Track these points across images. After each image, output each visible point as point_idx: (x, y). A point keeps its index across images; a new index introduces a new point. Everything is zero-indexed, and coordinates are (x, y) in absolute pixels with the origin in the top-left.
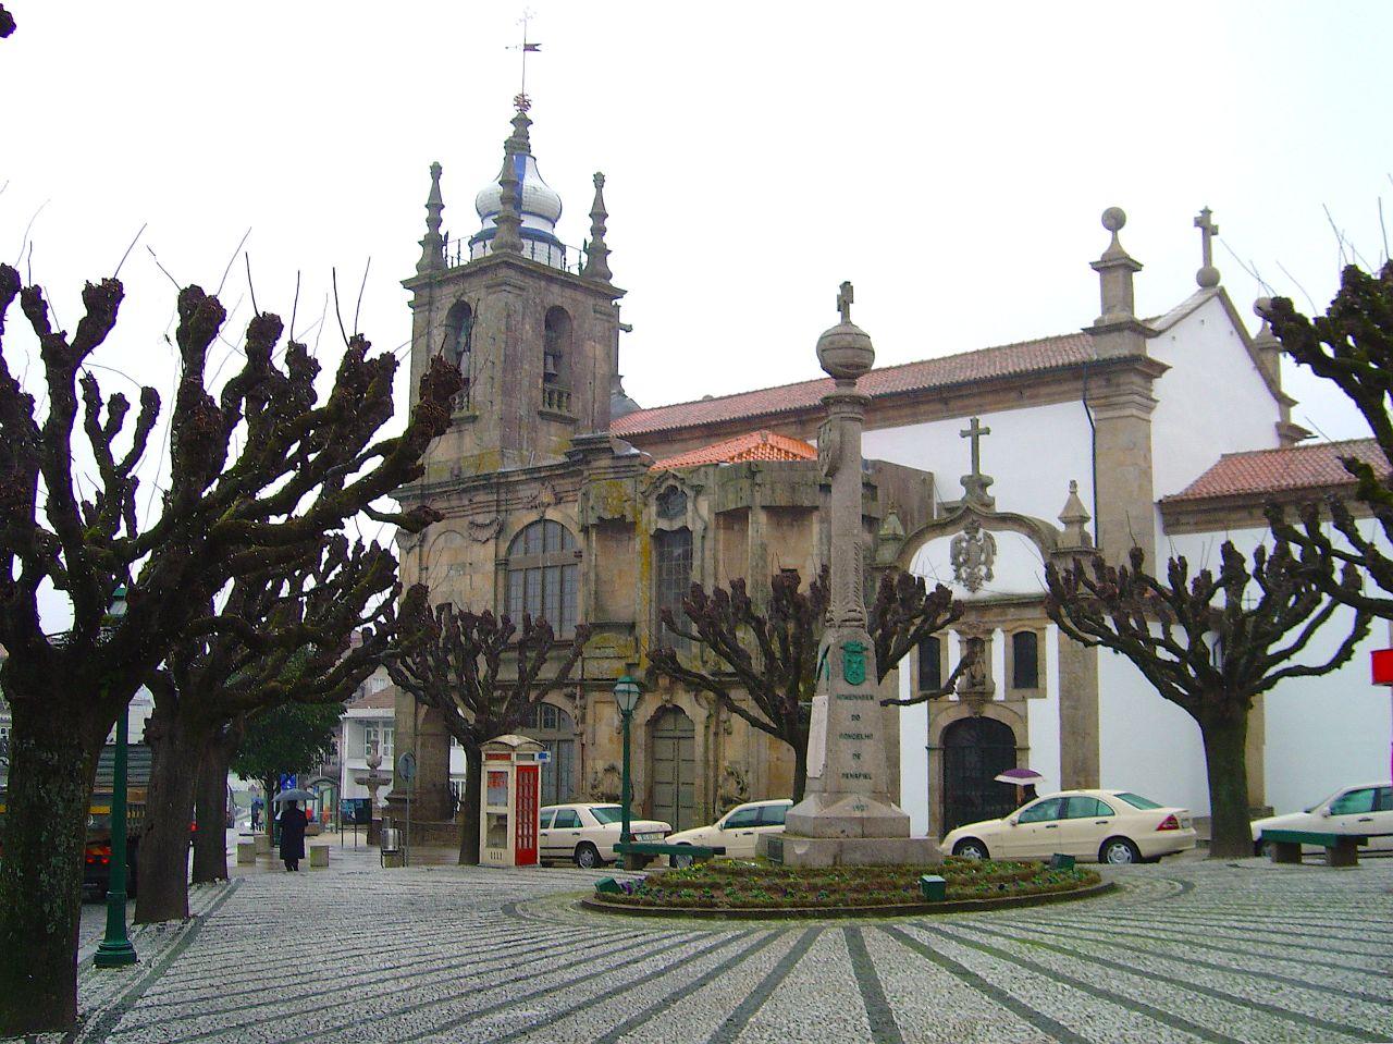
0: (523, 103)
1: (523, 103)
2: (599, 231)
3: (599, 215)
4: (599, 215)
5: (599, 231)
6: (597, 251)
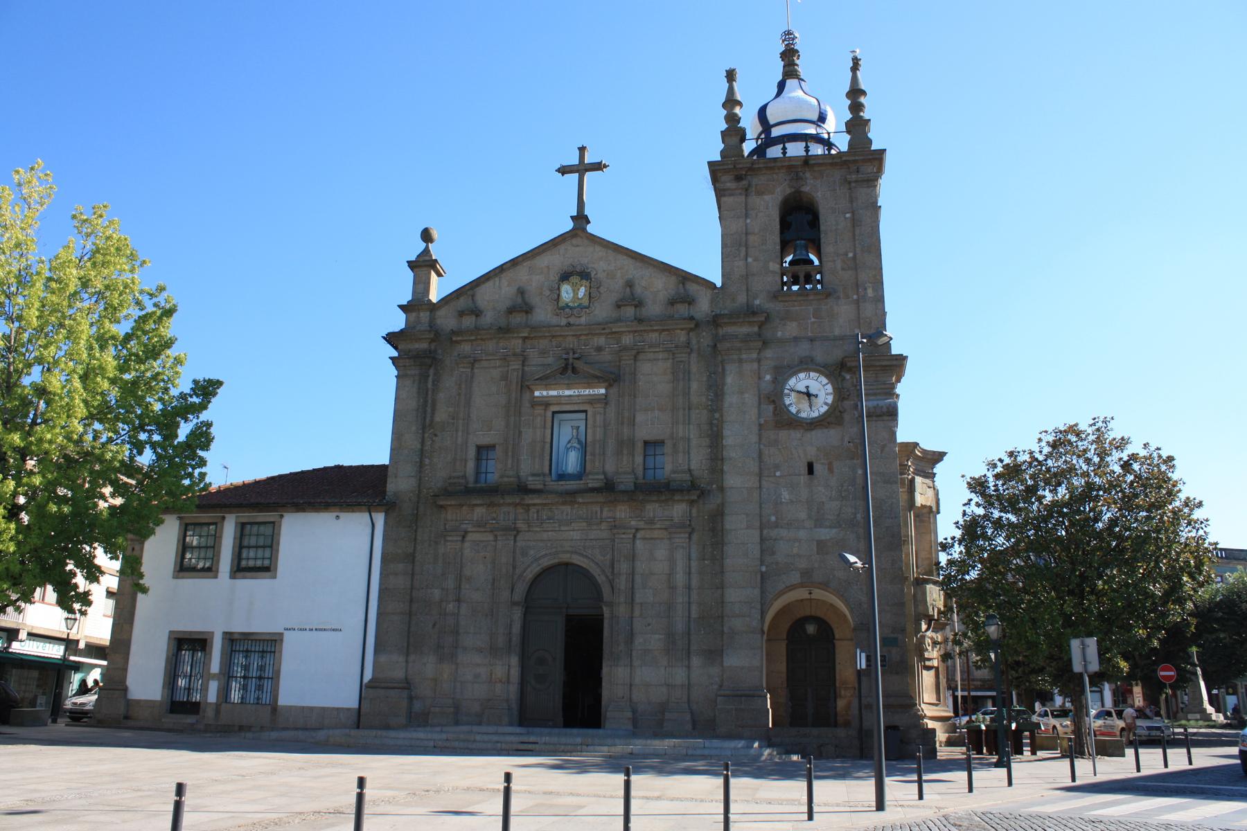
0: (788, 36)
1: (788, 36)
2: (856, 107)
3: (855, 93)
4: (855, 93)
5: (856, 107)
6: (857, 126)
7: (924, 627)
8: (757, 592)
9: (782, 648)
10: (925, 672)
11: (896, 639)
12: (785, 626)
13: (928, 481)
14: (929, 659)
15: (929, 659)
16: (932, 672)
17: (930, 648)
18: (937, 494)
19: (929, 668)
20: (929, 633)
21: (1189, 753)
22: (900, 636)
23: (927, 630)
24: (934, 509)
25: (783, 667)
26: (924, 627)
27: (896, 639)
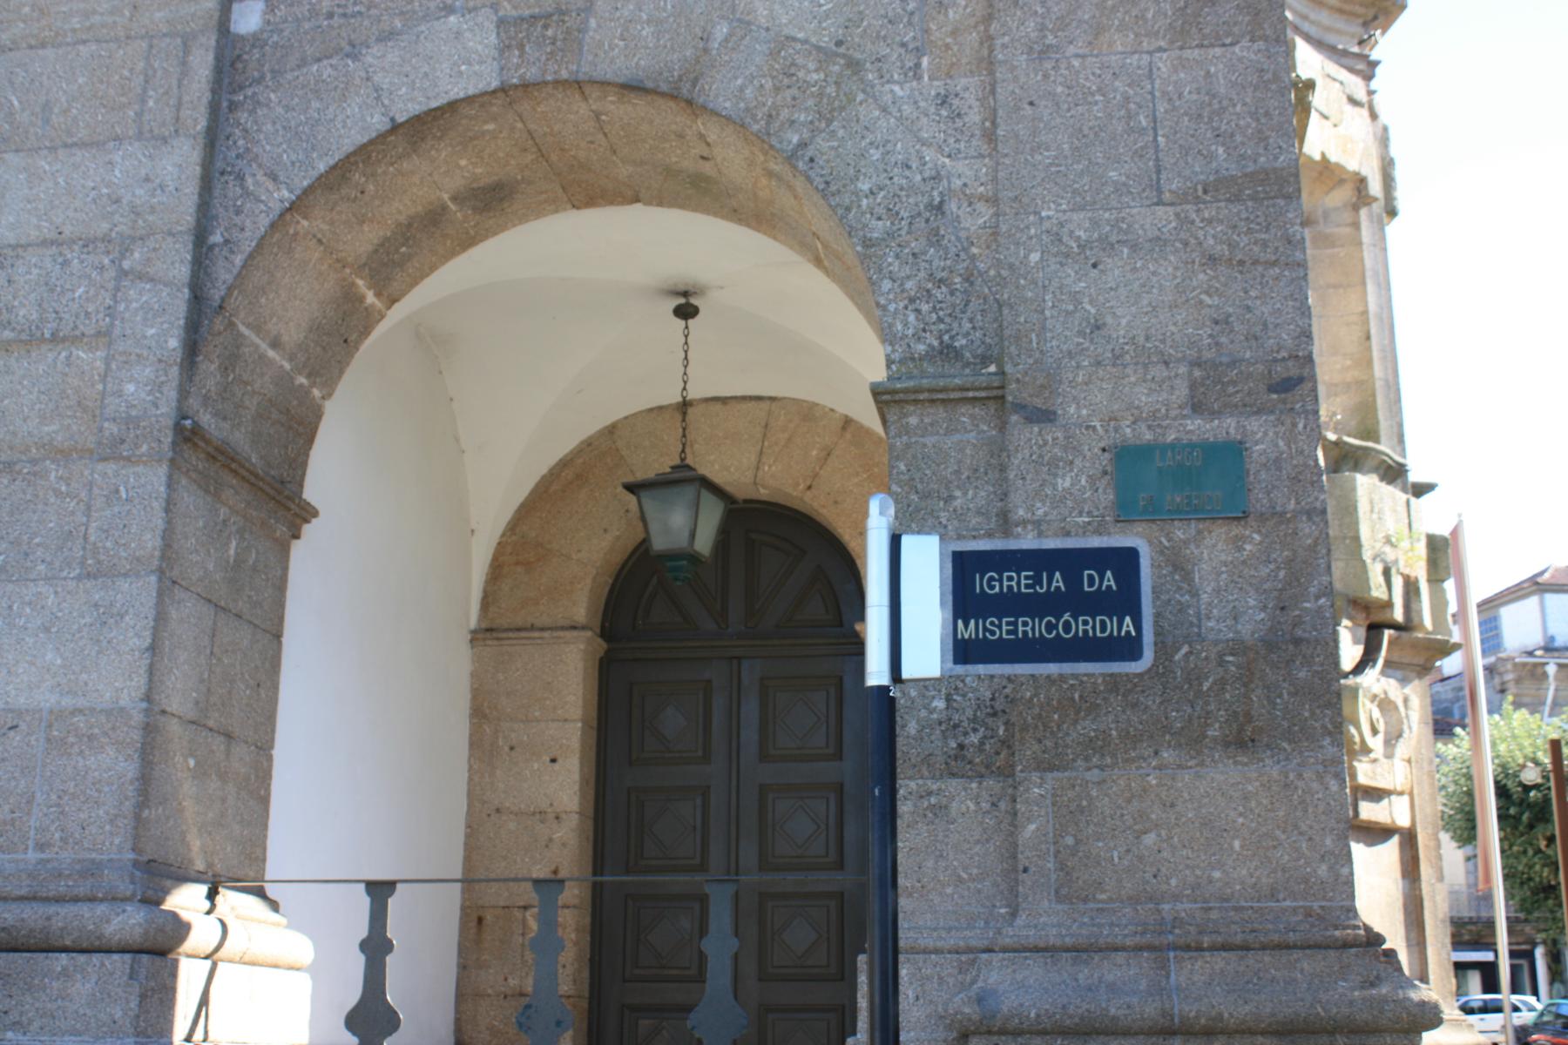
7: (1350, 651)
8: (179, 163)
9: (566, 676)
10: (1358, 850)
11: (1231, 453)
12: (592, 547)
13: (1356, 85)
14: (1376, 794)
15: (1376, 794)
16: (1390, 850)
17: (1376, 743)
18: (1384, 140)
19: (1377, 833)
20: (1372, 680)
21: (914, 951)
22: (1262, 436)
23: (1359, 669)
24: (1375, 187)
25: (560, 784)
26: (1350, 651)
27: (1231, 453)
